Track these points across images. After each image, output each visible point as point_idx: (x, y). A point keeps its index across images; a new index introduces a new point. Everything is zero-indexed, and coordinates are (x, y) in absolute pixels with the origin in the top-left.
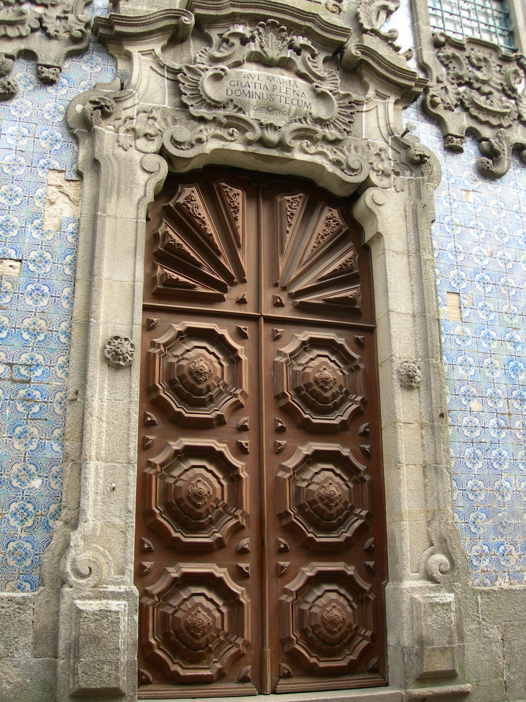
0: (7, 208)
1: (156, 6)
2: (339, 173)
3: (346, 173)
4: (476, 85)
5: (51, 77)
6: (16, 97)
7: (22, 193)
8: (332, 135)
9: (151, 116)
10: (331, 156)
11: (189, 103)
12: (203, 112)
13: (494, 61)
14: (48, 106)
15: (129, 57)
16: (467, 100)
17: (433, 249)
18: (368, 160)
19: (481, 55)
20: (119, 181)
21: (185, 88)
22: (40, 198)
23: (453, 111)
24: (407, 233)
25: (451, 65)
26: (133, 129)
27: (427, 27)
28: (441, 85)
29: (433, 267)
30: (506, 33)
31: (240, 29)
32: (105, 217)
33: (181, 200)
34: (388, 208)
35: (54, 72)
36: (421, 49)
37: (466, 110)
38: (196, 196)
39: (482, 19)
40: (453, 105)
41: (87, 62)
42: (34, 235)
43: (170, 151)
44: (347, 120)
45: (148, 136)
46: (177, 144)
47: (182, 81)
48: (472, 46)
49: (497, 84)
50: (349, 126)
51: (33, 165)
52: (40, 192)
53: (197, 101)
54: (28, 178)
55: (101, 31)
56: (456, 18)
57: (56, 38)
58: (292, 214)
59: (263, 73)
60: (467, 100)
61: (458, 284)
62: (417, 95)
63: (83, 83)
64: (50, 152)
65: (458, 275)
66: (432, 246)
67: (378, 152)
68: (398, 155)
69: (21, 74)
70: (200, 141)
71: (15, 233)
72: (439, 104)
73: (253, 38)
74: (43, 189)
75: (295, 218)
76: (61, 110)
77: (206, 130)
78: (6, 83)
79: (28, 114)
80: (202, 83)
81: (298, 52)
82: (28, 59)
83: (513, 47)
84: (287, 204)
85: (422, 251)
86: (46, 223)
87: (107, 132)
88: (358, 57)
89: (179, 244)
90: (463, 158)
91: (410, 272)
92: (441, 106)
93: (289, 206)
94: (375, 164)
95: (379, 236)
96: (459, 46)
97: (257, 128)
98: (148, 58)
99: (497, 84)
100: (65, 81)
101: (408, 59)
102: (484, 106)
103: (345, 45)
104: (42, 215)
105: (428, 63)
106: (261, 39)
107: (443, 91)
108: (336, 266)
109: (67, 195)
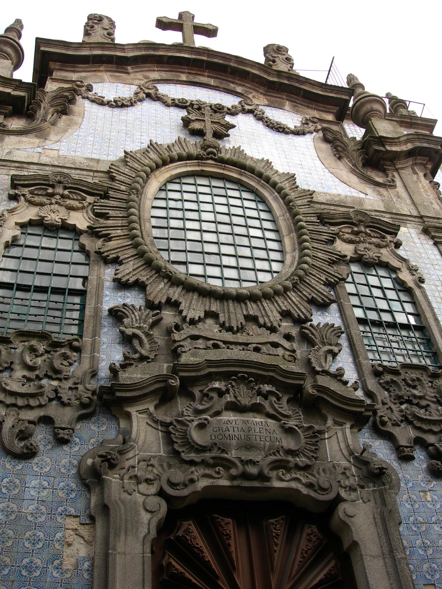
0: (31, 551)
1: (148, 373)
2: (312, 494)
3: (318, 493)
4: (415, 401)
5: (66, 437)
6: (38, 455)
7: (43, 538)
8: (303, 463)
9: (149, 463)
10: (304, 480)
11: (180, 450)
12: (193, 456)
13: (425, 379)
14: (63, 461)
15: (128, 416)
16: (409, 415)
17: (404, 548)
18: (336, 479)
19: (414, 376)
20: (126, 521)
21: (176, 438)
22: (59, 541)
23: (400, 426)
24: (379, 537)
25: (391, 389)
26: (136, 476)
27: (367, 361)
28: (386, 406)
29: (408, 564)
30: (431, 355)
31: (217, 385)
32: (115, 555)
33: (180, 533)
34: (359, 517)
35: (68, 433)
36: (365, 379)
37: (410, 423)
38: (193, 528)
39: (409, 347)
40: (399, 421)
41: (94, 423)
42: (55, 574)
43: (168, 492)
44: (313, 448)
45: (148, 481)
46: (172, 485)
47: (173, 432)
48: (405, 370)
49: (432, 397)
50: (316, 453)
51: (53, 513)
52: (59, 535)
53: (187, 447)
54: (48, 524)
55: (105, 397)
56: (388, 350)
57: (69, 405)
58: (277, 534)
59: (239, 418)
60: (409, 415)
61: (432, 575)
62: (368, 417)
63: (92, 441)
64: (67, 500)
65: (430, 567)
66: (403, 545)
67: (343, 471)
68: (360, 471)
69: (41, 436)
70: (192, 481)
71: (38, 573)
72: (387, 422)
73: (228, 391)
74: (62, 533)
75: (280, 538)
76: (75, 464)
77: (197, 471)
78: (29, 444)
79: (48, 469)
80: (190, 432)
81: (265, 396)
82: (47, 424)
83: (439, 365)
84: (272, 526)
85: (395, 551)
86: (65, 563)
87: (114, 480)
88: (315, 395)
89: (181, 573)
90: (415, 464)
91: (387, 572)
92: (389, 424)
93: (274, 528)
94: (342, 481)
95: (355, 544)
96: (394, 372)
97: (239, 464)
98: (143, 416)
99: (432, 397)
100: (77, 440)
101: (356, 389)
102: (425, 417)
103: (303, 386)
104: (61, 556)
105: (372, 390)
106: (234, 391)
107: (389, 411)
108: (321, 576)
109: (82, 537)
